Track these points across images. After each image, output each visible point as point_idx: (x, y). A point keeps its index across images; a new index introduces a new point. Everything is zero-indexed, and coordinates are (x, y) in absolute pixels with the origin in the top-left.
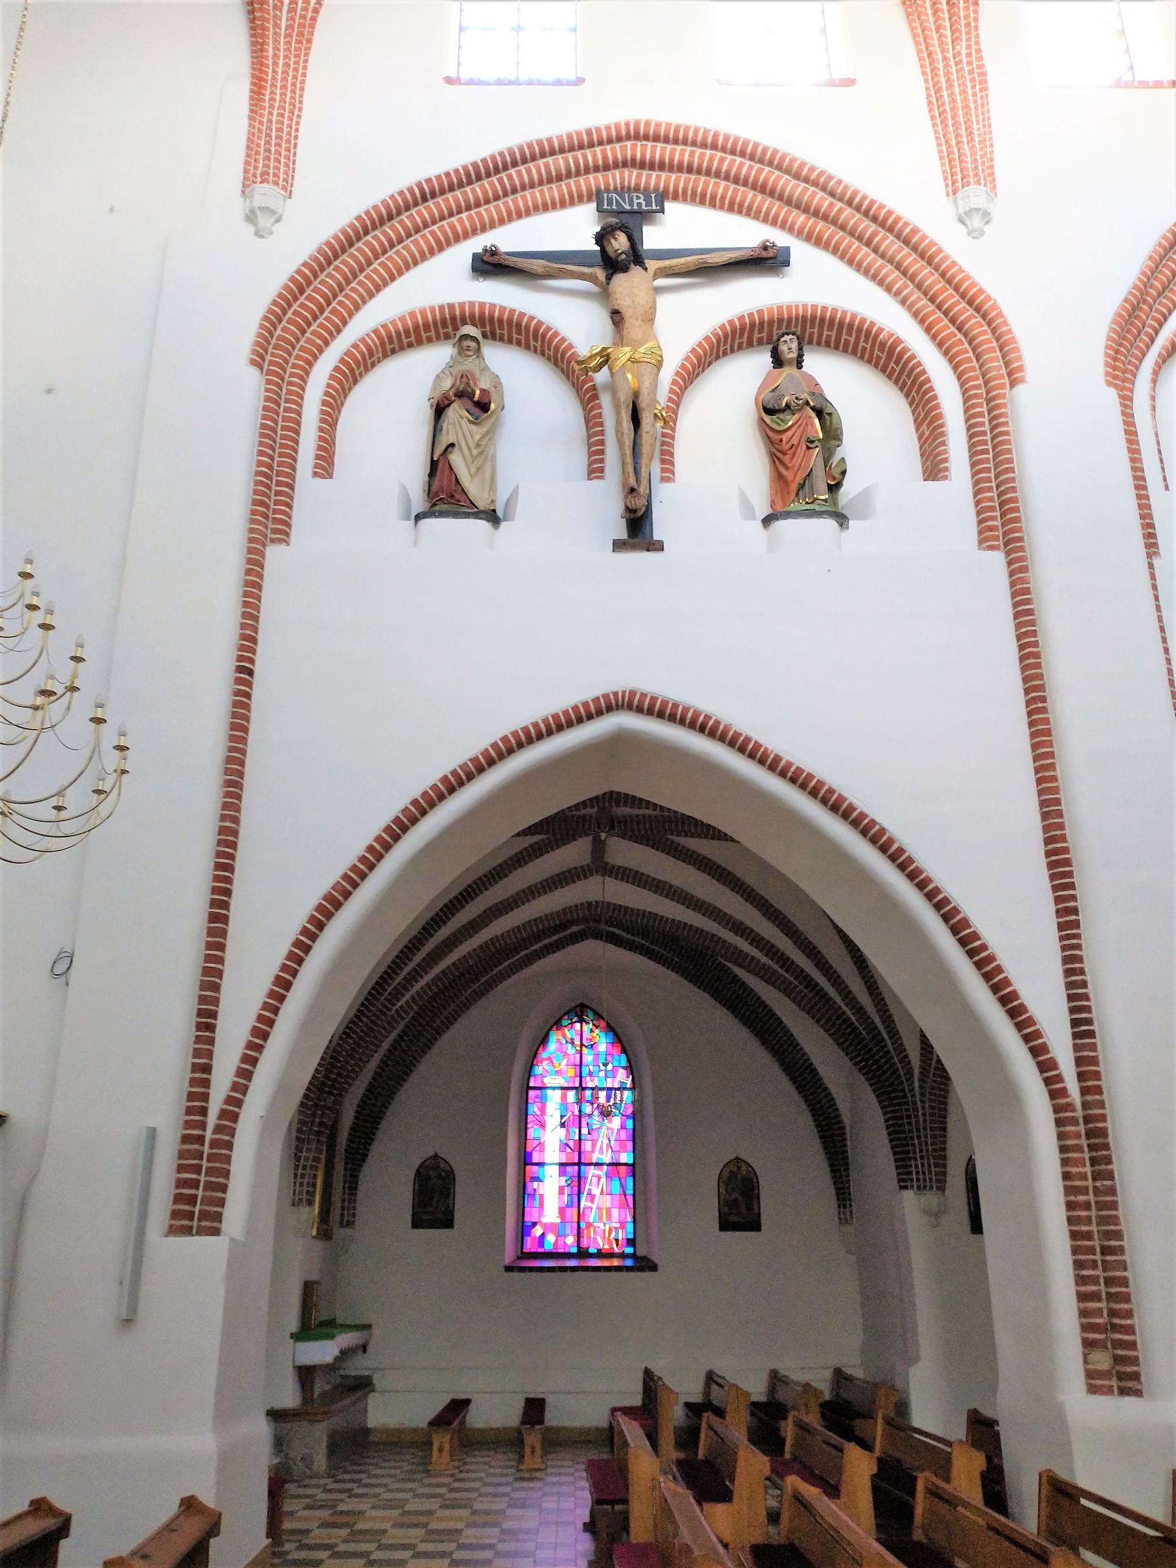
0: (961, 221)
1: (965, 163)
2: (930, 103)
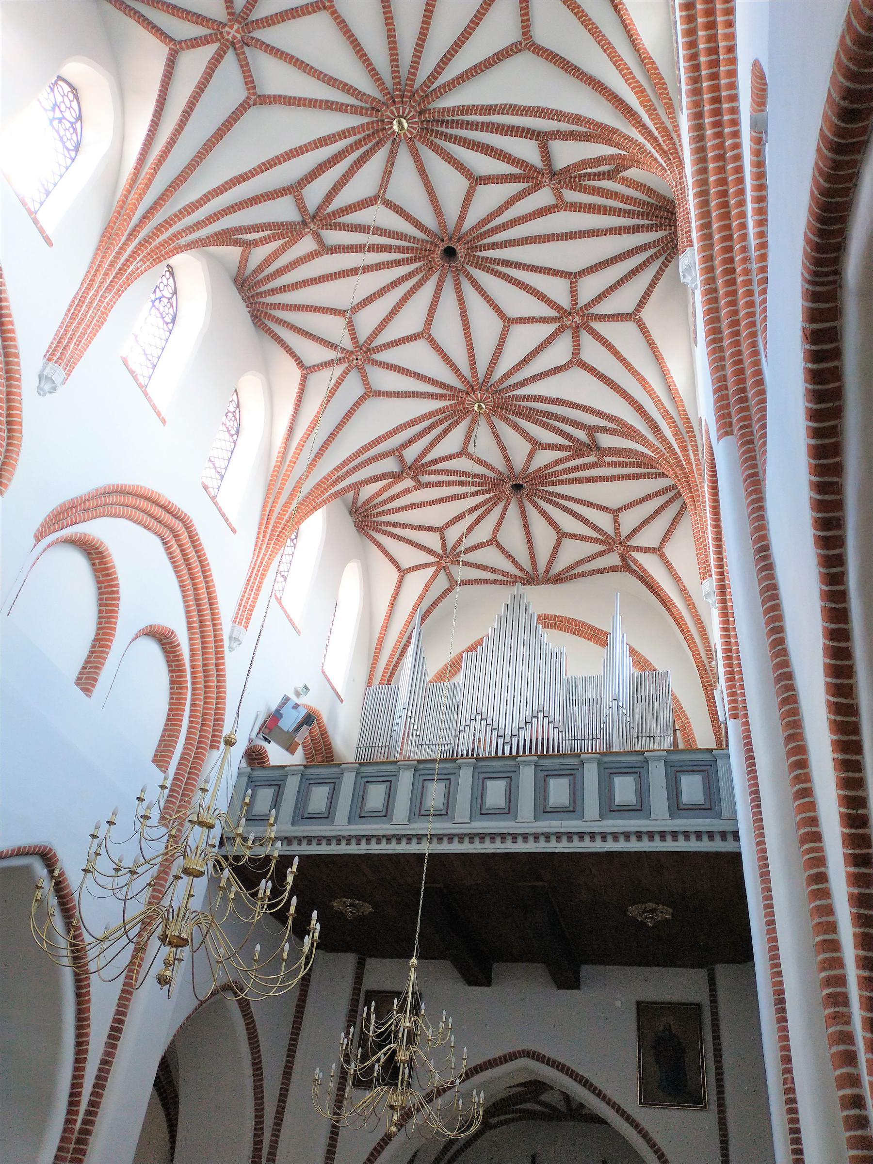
0: (40, 377)
1: (64, 350)
2: (73, 301)
